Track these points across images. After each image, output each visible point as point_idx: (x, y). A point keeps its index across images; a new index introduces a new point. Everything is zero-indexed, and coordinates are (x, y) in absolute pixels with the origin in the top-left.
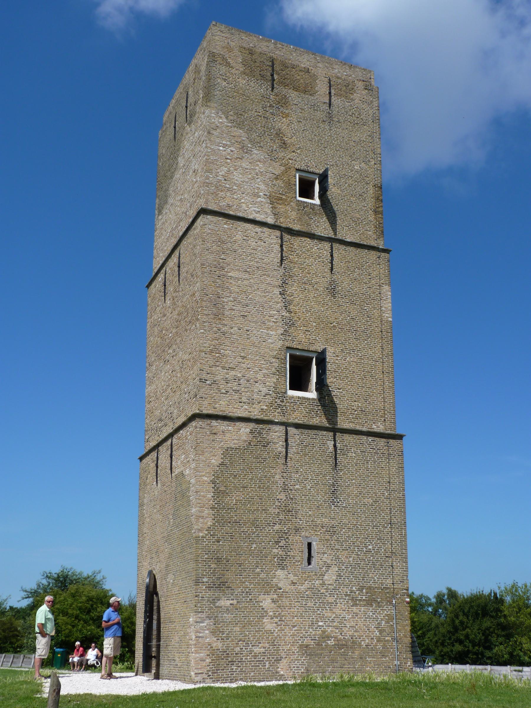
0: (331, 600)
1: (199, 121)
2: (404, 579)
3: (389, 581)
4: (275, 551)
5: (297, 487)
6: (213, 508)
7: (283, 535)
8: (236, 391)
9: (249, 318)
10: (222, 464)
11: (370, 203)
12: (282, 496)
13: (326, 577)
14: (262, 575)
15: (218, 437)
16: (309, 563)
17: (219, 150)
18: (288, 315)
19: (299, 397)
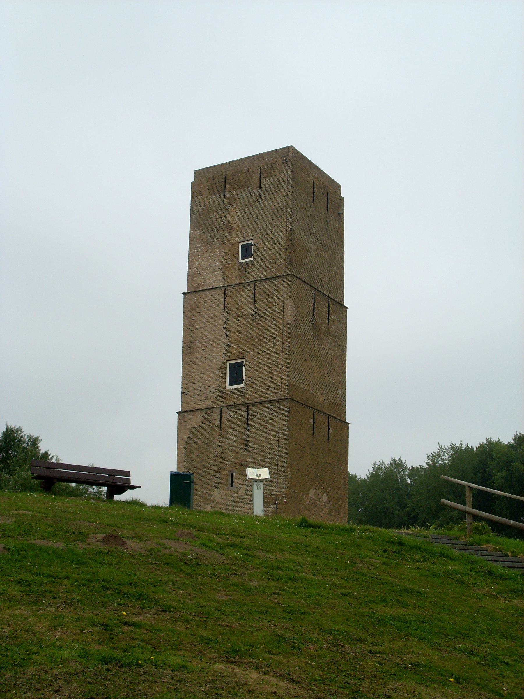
0: (242, 504)
1: (484, 584)
2: (253, 513)
3: (275, 490)
4: (214, 480)
5: (227, 443)
6: (184, 462)
7: (218, 471)
8: (199, 395)
9: (207, 349)
10: (189, 437)
11: (283, 244)
12: (218, 450)
13: (240, 492)
14: (207, 494)
15: (187, 423)
16: (232, 486)
17: (195, 252)
18: (228, 340)
19: (233, 389)
